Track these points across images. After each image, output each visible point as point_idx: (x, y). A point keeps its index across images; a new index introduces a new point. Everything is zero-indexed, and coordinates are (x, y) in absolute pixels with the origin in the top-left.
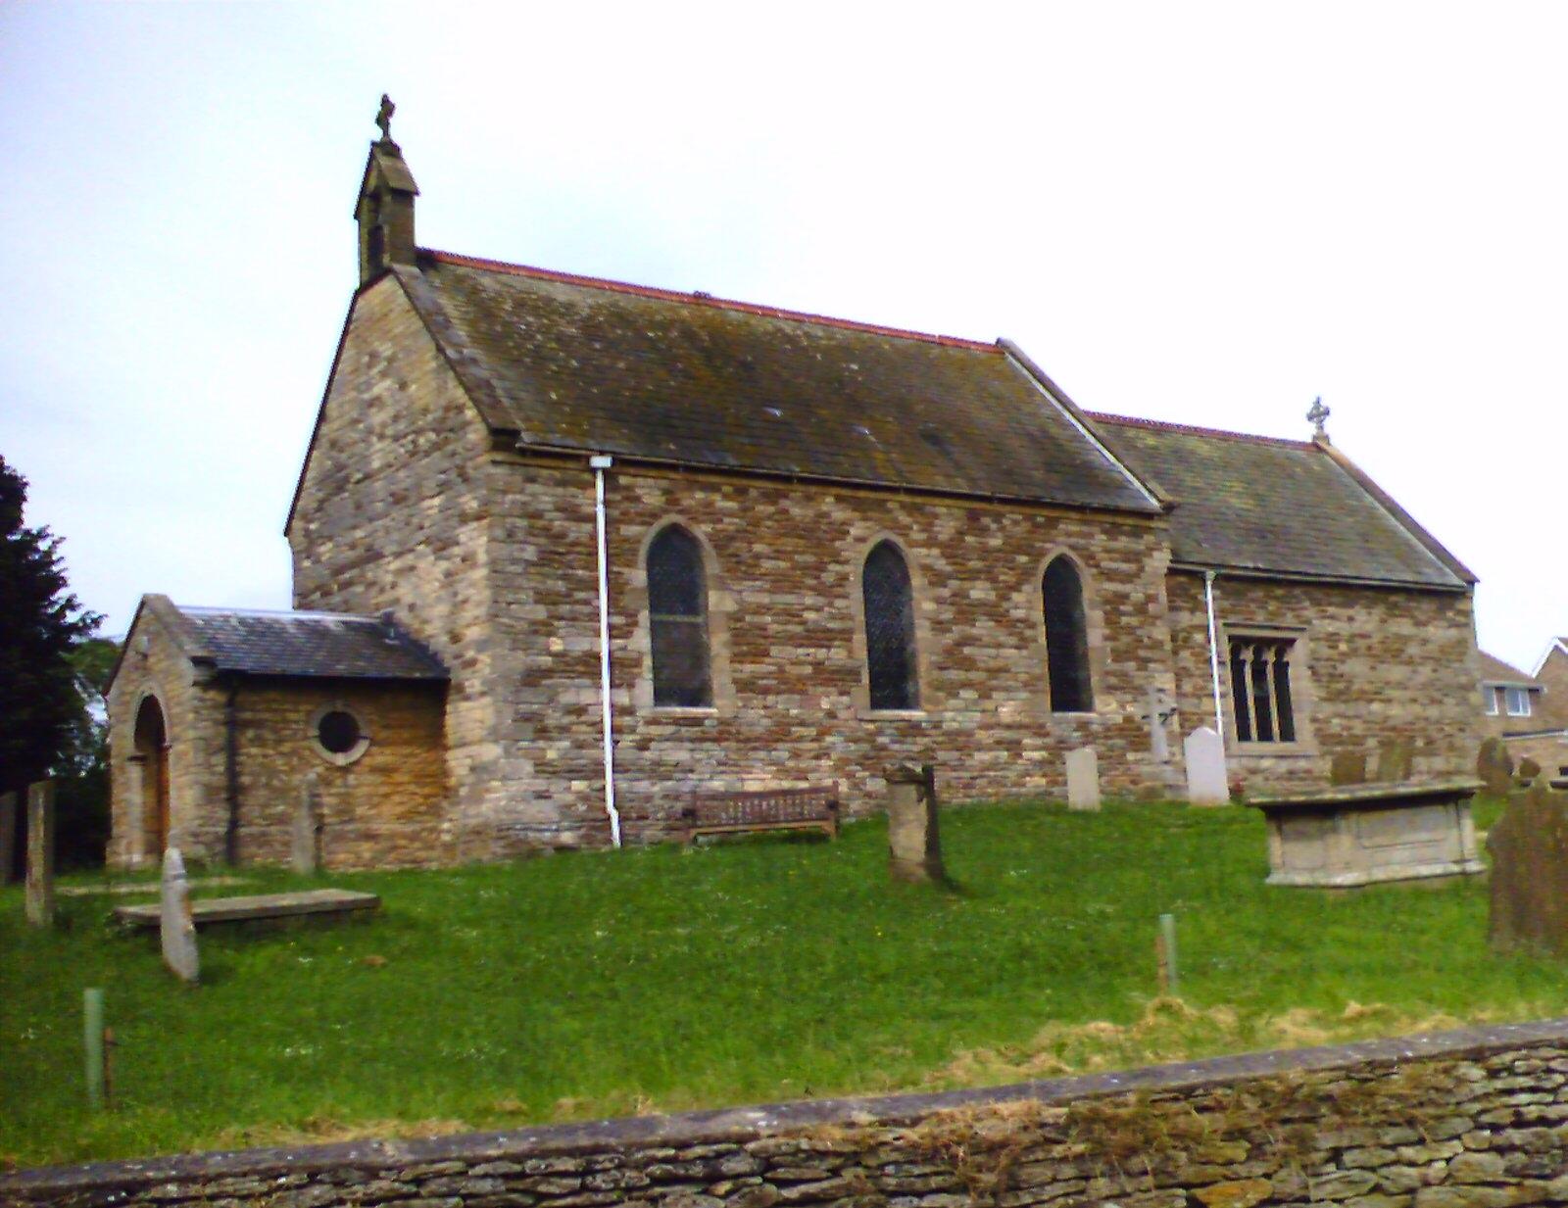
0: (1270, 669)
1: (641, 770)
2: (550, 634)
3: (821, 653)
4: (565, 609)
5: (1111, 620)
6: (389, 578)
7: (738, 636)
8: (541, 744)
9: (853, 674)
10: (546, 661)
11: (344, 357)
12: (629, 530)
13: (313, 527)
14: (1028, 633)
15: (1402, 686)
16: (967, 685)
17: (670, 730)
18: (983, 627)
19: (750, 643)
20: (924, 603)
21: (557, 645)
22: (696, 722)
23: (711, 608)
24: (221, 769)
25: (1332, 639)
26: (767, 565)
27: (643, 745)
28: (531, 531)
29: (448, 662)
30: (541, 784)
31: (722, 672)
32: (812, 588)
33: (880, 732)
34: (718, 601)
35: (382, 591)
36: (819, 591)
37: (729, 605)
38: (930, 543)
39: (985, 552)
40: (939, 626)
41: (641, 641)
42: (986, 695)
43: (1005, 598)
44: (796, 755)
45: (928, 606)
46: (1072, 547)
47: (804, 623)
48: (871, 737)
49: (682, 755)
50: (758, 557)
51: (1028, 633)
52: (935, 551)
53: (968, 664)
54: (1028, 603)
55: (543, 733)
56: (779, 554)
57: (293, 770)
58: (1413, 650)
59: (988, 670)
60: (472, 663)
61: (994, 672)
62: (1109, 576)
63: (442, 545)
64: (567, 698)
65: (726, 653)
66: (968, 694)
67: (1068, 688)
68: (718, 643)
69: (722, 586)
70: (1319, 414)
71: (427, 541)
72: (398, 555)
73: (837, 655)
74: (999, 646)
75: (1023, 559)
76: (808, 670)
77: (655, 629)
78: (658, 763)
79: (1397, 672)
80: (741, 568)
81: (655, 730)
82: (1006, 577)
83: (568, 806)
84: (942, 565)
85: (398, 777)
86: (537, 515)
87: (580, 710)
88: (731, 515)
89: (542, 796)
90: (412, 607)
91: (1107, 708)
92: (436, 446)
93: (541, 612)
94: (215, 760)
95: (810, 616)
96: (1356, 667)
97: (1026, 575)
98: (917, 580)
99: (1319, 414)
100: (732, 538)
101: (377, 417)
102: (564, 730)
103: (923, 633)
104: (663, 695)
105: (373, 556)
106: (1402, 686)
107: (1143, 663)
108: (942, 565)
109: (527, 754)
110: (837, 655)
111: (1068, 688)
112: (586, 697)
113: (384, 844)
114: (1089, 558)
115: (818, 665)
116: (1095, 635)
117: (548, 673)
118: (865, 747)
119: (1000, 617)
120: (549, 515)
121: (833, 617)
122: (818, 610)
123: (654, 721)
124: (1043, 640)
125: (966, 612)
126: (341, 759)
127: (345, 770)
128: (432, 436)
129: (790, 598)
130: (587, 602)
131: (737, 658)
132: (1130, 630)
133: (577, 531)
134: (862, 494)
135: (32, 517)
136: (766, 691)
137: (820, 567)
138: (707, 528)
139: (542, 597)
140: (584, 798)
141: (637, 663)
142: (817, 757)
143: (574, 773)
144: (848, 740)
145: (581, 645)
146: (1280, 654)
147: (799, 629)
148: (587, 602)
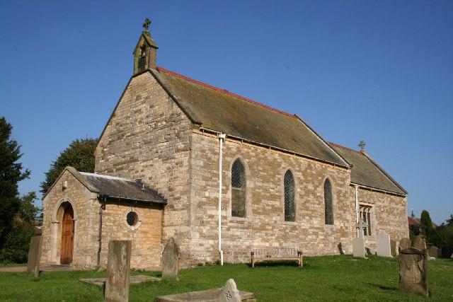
0: (367, 215)
1: (228, 237)
2: (206, 191)
3: (274, 203)
4: (210, 183)
5: (339, 197)
6: (141, 168)
7: (254, 195)
8: (202, 227)
9: (280, 210)
10: (204, 200)
11: (125, 96)
12: (228, 159)
13: (105, 149)
14: (321, 200)
15: (393, 221)
16: (307, 215)
17: (235, 225)
18: (311, 198)
19: (257, 199)
20: (298, 189)
21: (207, 194)
22: (242, 223)
23: (247, 186)
24: (97, 229)
25: (380, 207)
26: (262, 173)
27: (228, 229)
28: (202, 156)
29: (166, 196)
30: (202, 241)
31: (249, 207)
32: (272, 182)
33: (287, 228)
34: (250, 184)
35: (137, 172)
36: (274, 183)
37: (252, 186)
38: (299, 171)
39: (312, 175)
40: (302, 197)
41: (229, 195)
42: (311, 219)
43: (315, 189)
44: (266, 234)
45: (299, 190)
46: (331, 176)
47: (270, 192)
48: (285, 230)
49: (239, 233)
50: (260, 170)
51: (321, 200)
52: (301, 173)
53: (307, 208)
54: (320, 191)
55: (202, 223)
56: (264, 171)
57: (118, 231)
58: (395, 212)
59: (312, 211)
60: (179, 198)
61: (313, 211)
62: (339, 185)
63: (166, 159)
64: (209, 212)
65: (251, 200)
66: (307, 218)
67: (329, 220)
68: (249, 197)
69: (251, 179)
70: (362, 144)
71: (160, 157)
72: (144, 161)
73: (277, 204)
74: (314, 203)
75: (320, 178)
76: (270, 208)
77: (233, 191)
78: (233, 235)
79: (392, 218)
80: (255, 174)
81: (231, 224)
82: (316, 183)
83: (208, 248)
84: (302, 178)
85: (148, 235)
86: (204, 151)
87: (212, 217)
88: (254, 157)
89: (201, 245)
90: (150, 178)
91: (337, 224)
92: (165, 127)
93: (204, 183)
94: (95, 226)
95: (272, 190)
96: (384, 215)
97: (320, 184)
98: (296, 182)
99: (362, 144)
100: (253, 164)
101: (139, 117)
102: (208, 222)
103: (297, 198)
104: (234, 214)
105: (133, 160)
106: (393, 221)
107: (345, 211)
108: (302, 178)
109: (198, 231)
110: (277, 204)
111: (329, 220)
112: (213, 213)
113: (144, 258)
114: (334, 179)
115: (273, 206)
116: (335, 202)
117: (204, 204)
118: (283, 233)
119: (314, 194)
120: (207, 152)
121: (277, 192)
122: (274, 189)
123: (231, 222)
124: (324, 203)
125: (308, 192)
126: (133, 228)
127: (134, 232)
128: (164, 123)
129: (266, 185)
130: (216, 181)
131: (253, 203)
132: (342, 201)
133: (214, 158)
134: (285, 154)
135: (12, 137)
136: (260, 214)
137: (274, 176)
138: (247, 160)
139: (205, 179)
140: (212, 246)
141: (228, 202)
142: (272, 235)
143: (210, 237)
144: (280, 230)
145: (213, 196)
146: (369, 210)
147: (269, 195)
148: (216, 181)
